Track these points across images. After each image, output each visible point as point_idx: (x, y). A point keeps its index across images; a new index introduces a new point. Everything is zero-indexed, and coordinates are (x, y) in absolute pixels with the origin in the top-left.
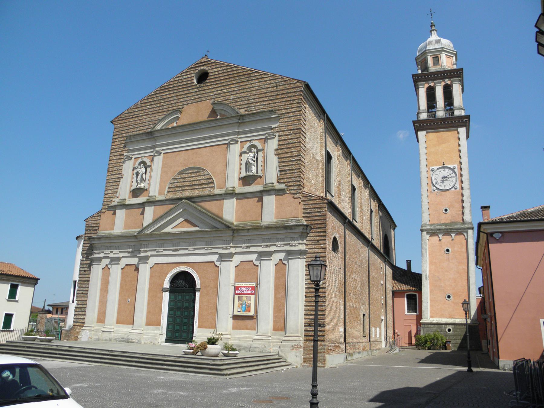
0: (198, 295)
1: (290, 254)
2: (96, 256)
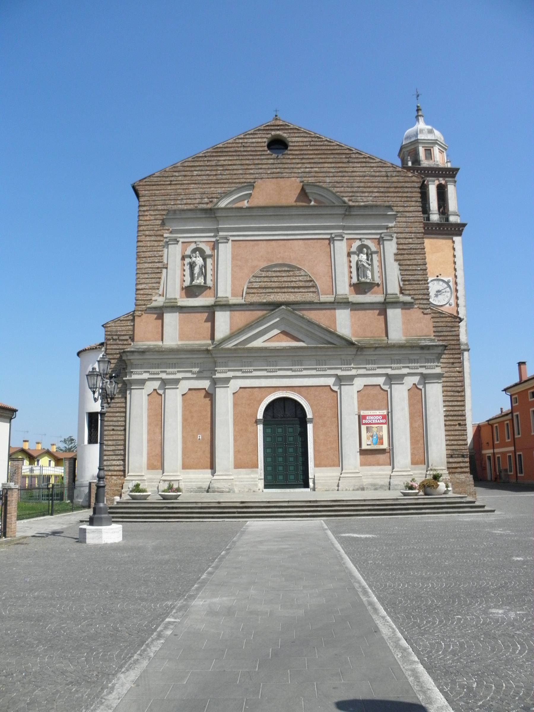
0: (310, 427)
1: (425, 378)
2: (134, 377)
